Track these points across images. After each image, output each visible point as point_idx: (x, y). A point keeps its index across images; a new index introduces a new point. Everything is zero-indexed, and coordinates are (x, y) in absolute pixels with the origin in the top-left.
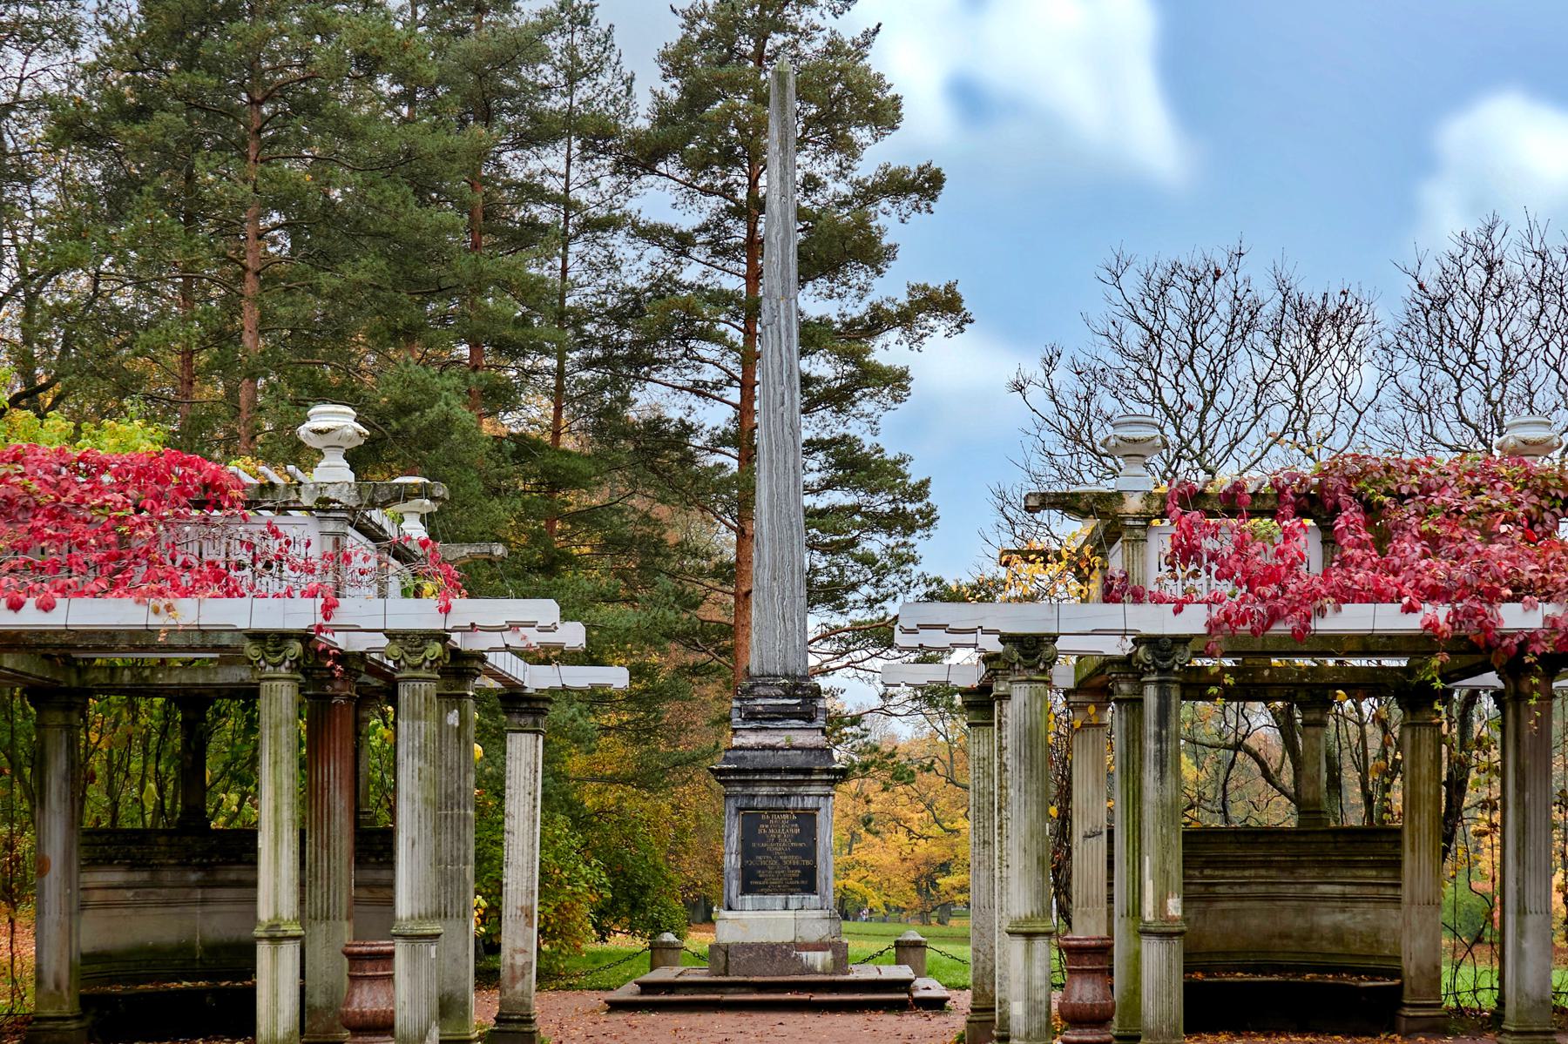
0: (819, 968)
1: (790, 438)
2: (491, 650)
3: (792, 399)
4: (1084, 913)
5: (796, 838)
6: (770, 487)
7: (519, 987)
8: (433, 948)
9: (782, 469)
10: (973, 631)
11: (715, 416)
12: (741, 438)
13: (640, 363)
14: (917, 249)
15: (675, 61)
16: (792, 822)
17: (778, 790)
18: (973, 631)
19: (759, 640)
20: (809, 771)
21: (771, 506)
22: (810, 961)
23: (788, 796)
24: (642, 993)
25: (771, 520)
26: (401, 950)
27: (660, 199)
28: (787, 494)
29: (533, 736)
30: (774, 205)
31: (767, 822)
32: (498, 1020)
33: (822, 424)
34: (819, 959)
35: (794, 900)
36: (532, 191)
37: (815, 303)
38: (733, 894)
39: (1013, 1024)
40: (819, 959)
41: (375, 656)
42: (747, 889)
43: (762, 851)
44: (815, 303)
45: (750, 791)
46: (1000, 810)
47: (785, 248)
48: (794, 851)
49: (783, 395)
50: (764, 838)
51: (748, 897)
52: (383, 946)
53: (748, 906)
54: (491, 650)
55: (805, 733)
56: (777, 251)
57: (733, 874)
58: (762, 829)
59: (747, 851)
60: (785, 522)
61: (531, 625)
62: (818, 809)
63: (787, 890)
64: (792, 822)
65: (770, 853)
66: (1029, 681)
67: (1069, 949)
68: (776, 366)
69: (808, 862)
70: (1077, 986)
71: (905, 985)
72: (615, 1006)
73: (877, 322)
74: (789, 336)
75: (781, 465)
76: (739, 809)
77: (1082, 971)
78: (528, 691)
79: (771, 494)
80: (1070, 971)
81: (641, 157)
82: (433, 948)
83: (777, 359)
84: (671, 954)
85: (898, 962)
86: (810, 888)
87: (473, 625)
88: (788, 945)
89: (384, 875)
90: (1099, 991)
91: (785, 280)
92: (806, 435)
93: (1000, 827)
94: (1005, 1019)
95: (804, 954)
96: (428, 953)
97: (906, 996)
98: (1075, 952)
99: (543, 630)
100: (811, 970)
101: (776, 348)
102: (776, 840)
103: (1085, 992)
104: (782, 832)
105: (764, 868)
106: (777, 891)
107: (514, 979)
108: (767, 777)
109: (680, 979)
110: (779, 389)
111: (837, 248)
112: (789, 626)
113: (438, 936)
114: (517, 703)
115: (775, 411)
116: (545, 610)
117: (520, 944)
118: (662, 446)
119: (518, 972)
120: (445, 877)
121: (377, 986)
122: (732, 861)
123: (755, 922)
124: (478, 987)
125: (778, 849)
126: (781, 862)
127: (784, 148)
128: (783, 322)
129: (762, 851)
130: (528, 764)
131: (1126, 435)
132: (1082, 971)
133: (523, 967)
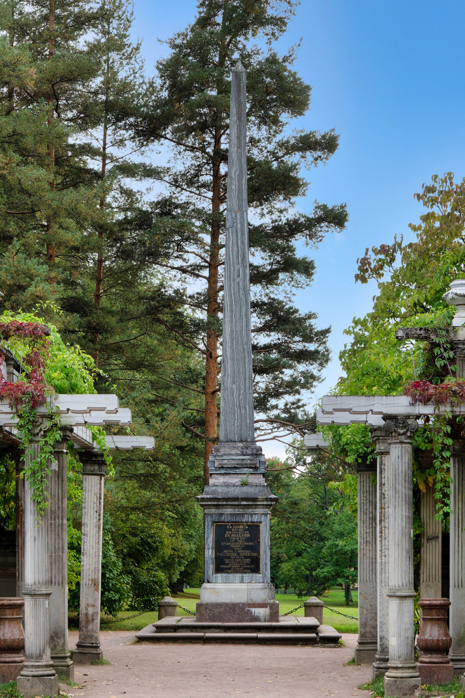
0: (262, 618)
1: (243, 297)
2: (78, 425)
3: (244, 273)
4: (427, 586)
5: (248, 540)
6: (231, 327)
7: (90, 627)
8: (47, 602)
9: (238, 315)
10: (367, 413)
11: (197, 286)
12: (210, 300)
13: (154, 255)
14: (320, 183)
15: (170, 69)
16: (245, 530)
17: (237, 511)
18: (367, 413)
19: (225, 420)
20: (255, 499)
21: (232, 339)
22: (257, 614)
23: (243, 515)
24: (155, 632)
25: (232, 347)
26: (28, 603)
27: (164, 153)
28: (241, 331)
29: (98, 477)
30: (233, 156)
31: (230, 530)
32: (78, 646)
33: (257, 292)
34: (261, 612)
35: (247, 576)
36: (87, 149)
37: (256, 217)
38: (210, 572)
39: (391, 650)
40: (261, 612)
41: (7, 429)
42: (218, 570)
43: (228, 548)
44: (256, 217)
45: (220, 511)
46: (381, 521)
47: (240, 180)
48: (246, 548)
49: (239, 271)
50: (228, 540)
51: (219, 575)
52: (15, 600)
53: (219, 580)
54: (78, 425)
55: (253, 476)
56: (235, 182)
57: (210, 561)
58: (227, 534)
59: (218, 547)
60: (240, 348)
61: (102, 409)
62: (260, 522)
63: (243, 570)
64: (245, 530)
65: (232, 549)
66: (401, 443)
67: (424, 607)
68: (235, 253)
69: (255, 554)
70: (429, 628)
71: (313, 629)
72: (141, 640)
73: (294, 228)
74: (243, 234)
75: (238, 314)
76: (214, 522)
77: (431, 620)
78: (96, 450)
79: (232, 332)
80: (424, 619)
81: (149, 131)
82: (47, 602)
83: (235, 248)
84: (170, 609)
85: (306, 615)
86: (256, 570)
87: (68, 410)
88: (243, 604)
89: (10, 559)
90: (442, 632)
91: (240, 199)
92: (252, 298)
93: (381, 532)
94: (385, 650)
95: (253, 610)
96: (44, 605)
97: (314, 635)
98: (427, 608)
99: (110, 412)
100: (257, 619)
101: (235, 241)
102: (236, 541)
103: (432, 633)
104: (239, 536)
105: (229, 557)
106: (236, 571)
107: (87, 622)
108: (230, 503)
109: (180, 624)
110: (237, 267)
111: (270, 182)
112: (243, 411)
113: (49, 595)
114: (90, 458)
115: (234, 280)
116: (110, 401)
117: (91, 602)
118: (162, 306)
119: (90, 618)
120: (54, 560)
121: (13, 624)
122: (209, 553)
123: (225, 589)
124: (69, 627)
125: (237, 546)
126: (238, 554)
127: (239, 119)
128: (239, 226)
129: (228, 548)
130: (96, 494)
131: (459, 292)
132: (431, 620)
133: (93, 615)
